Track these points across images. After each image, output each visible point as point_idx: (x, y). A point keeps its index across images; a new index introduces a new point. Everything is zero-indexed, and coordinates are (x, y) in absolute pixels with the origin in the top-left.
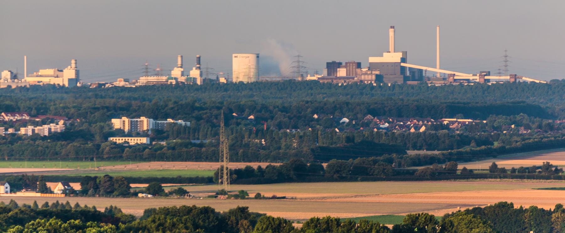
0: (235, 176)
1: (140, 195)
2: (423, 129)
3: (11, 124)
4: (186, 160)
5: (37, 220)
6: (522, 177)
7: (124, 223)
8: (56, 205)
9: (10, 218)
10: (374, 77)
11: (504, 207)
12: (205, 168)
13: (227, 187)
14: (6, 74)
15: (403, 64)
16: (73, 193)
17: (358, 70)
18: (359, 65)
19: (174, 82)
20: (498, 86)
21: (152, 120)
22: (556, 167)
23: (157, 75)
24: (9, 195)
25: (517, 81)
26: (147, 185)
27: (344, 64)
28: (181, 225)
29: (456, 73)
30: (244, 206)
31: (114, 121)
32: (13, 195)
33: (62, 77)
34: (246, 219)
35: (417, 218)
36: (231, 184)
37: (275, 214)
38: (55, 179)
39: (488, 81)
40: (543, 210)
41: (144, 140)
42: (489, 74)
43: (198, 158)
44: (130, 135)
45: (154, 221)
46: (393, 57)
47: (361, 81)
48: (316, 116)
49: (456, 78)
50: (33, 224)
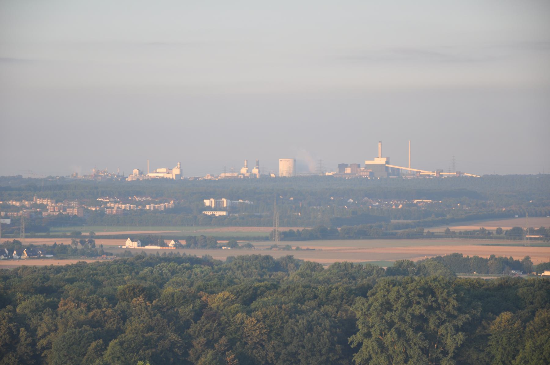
0: (283, 236)
1: (223, 248)
2: (400, 206)
3: (140, 203)
4: (251, 226)
5: (162, 264)
6: (466, 237)
7: (217, 265)
8: (171, 254)
9: (144, 262)
10: (368, 173)
11: (457, 256)
12: (264, 231)
13: (278, 243)
14: (136, 171)
15: (387, 165)
16: (181, 246)
17: (358, 169)
18: (359, 166)
19: (242, 176)
20: (449, 178)
21: (229, 200)
22: (489, 231)
23: (232, 172)
24: (140, 248)
25: (461, 175)
26: (227, 242)
27: (349, 165)
28: (253, 267)
29: (421, 171)
30: (291, 255)
31: (205, 201)
32: (143, 248)
33: (172, 173)
34: (292, 262)
35: (402, 263)
36: (280, 240)
37: (312, 260)
38: (170, 238)
39: (442, 175)
40: (482, 259)
41: (224, 213)
42: (442, 171)
43: (259, 225)
44: (215, 210)
45: (235, 264)
46: (381, 161)
47: (360, 176)
48: (332, 198)
49: (421, 174)
50: (159, 266)
